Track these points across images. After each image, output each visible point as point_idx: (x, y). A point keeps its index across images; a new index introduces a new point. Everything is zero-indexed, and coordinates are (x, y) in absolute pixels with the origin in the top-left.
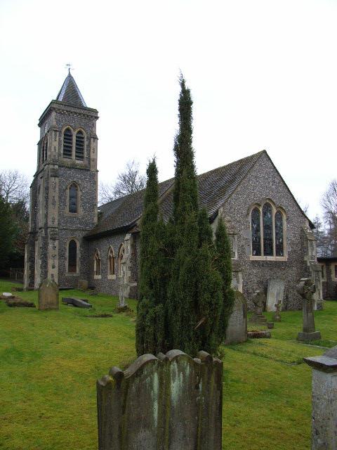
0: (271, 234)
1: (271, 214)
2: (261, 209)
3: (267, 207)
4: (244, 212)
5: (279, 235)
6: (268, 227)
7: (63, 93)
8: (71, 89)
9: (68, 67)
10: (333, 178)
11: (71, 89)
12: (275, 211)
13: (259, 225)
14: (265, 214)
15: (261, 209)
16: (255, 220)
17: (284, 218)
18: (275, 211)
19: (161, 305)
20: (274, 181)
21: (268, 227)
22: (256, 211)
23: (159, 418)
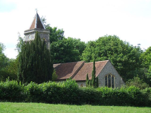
0: (111, 82)
1: (110, 77)
2: (108, 76)
3: (109, 76)
4: (103, 77)
5: (113, 82)
6: (109, 81)
7: (36, 22)
8: (39, 23)
9: (36, 10)
10: (150, 46)
11: (39, 23)
12: (111, 76)
13: (107, 80)
14: (109, 77)
15: (108, 76)
16: (106, 79)
17: (114, 78)
18: (111, 76)
19: (96, 77)
20: (112, 68)
21: (109, 81)
22: (106, 77)
23: (61, 79)
